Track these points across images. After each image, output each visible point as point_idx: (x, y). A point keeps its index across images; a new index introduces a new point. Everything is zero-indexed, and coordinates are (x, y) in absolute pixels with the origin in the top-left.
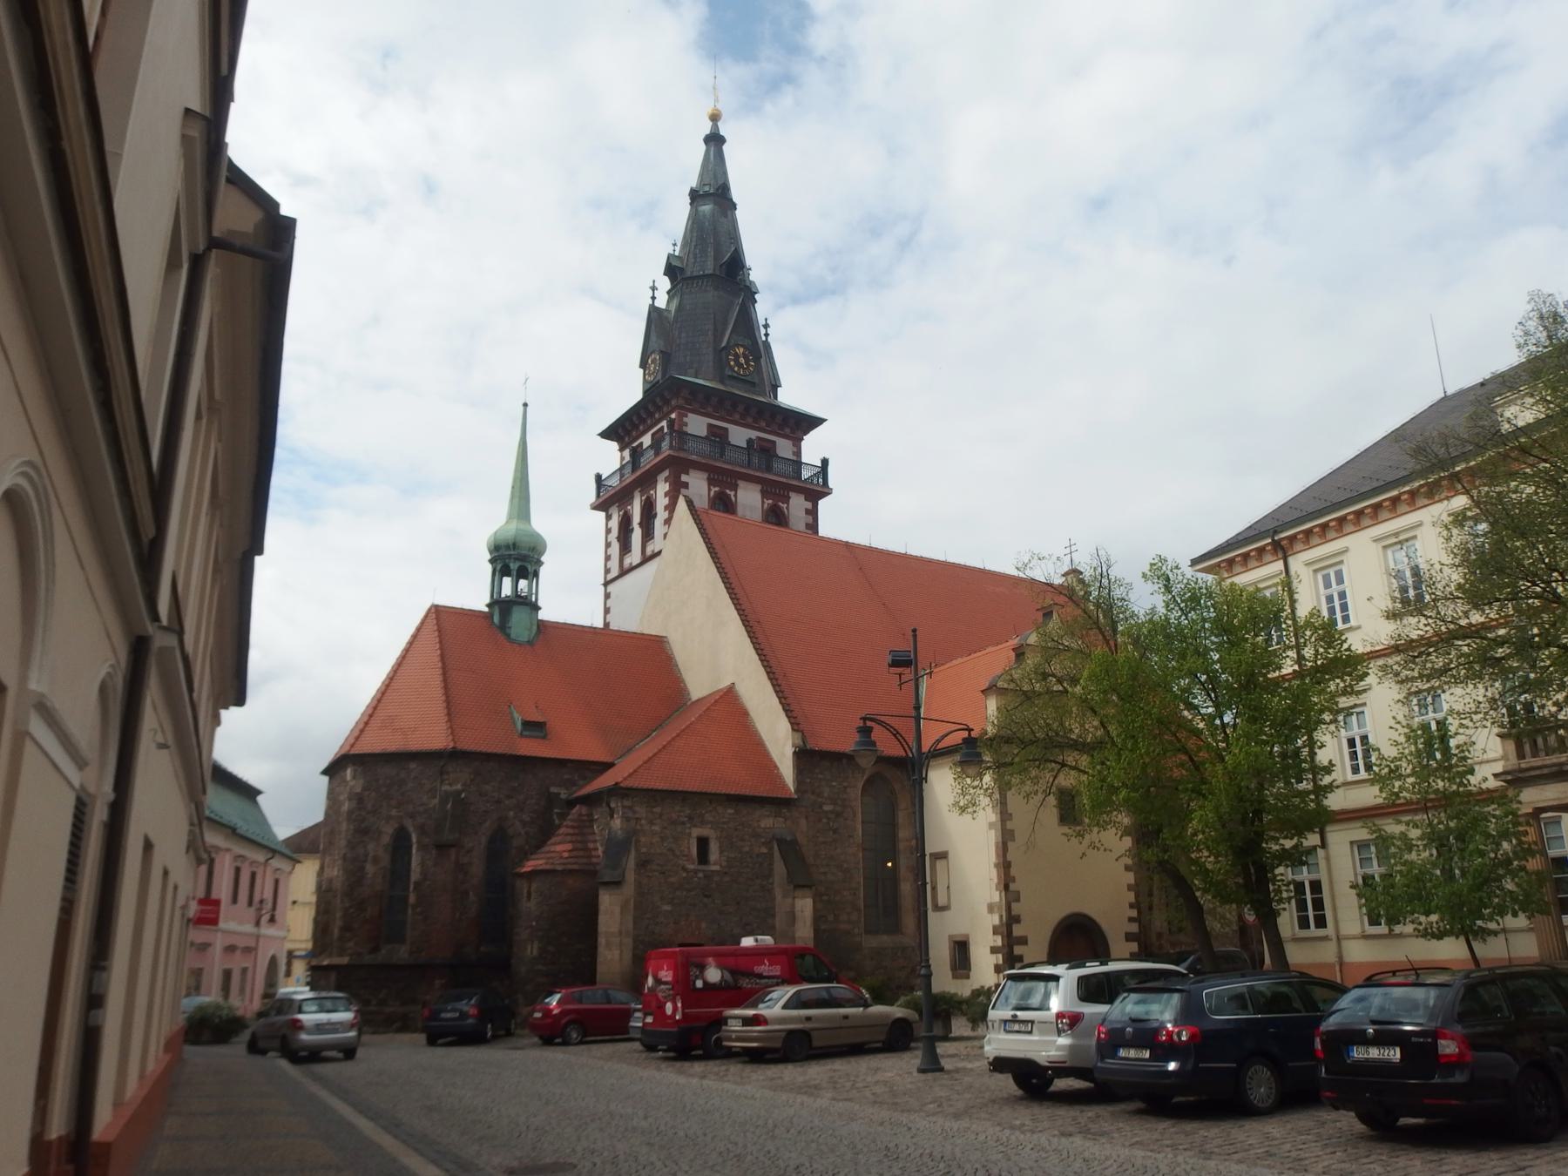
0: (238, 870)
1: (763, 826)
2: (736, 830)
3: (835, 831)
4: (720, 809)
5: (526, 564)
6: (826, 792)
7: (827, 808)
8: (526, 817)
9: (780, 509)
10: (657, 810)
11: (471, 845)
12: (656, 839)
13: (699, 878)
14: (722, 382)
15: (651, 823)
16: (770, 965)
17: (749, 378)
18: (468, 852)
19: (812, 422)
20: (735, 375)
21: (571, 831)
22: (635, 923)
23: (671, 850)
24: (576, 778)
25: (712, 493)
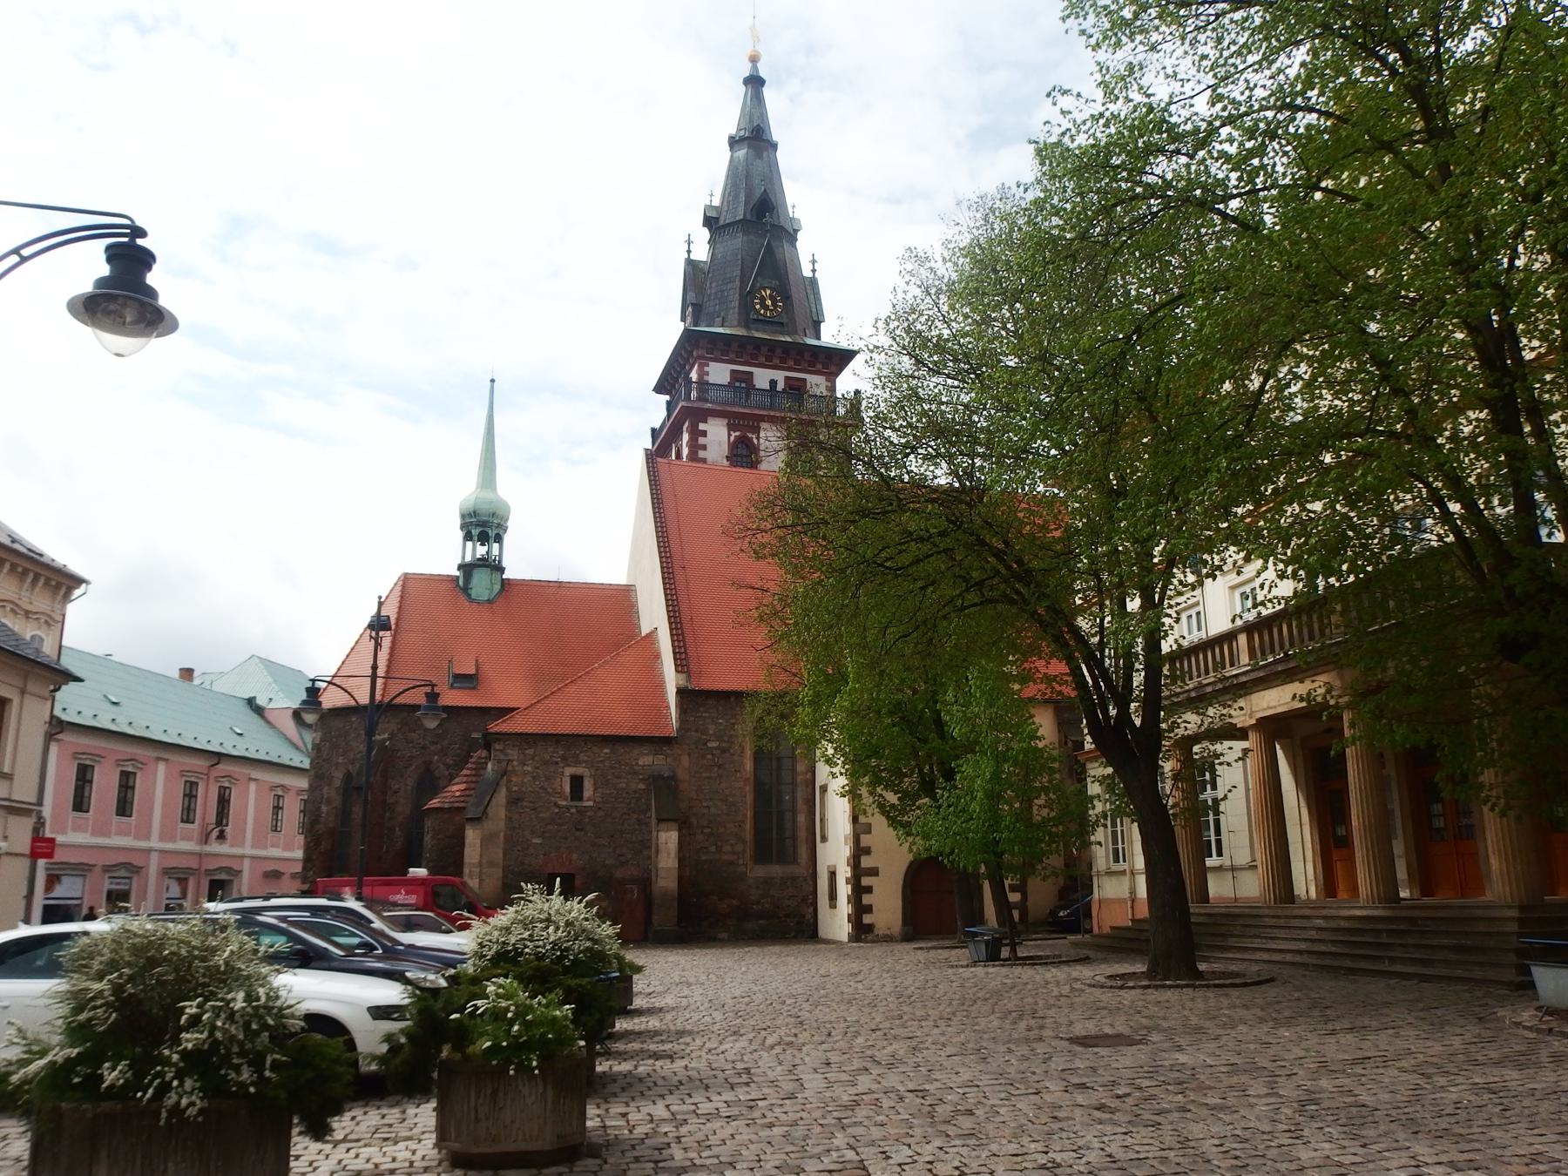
1: (641, 763)
3: (720, 766)
4: (596, 749)
6: (712, 729)
7: (711, 745)
8: (449, 761)
10: (530, 751)
12: (528, 779)
14: (747, 327)
16: (407, 894)
17: (776, 320)
22: (505, 854)
25: (732, 438)
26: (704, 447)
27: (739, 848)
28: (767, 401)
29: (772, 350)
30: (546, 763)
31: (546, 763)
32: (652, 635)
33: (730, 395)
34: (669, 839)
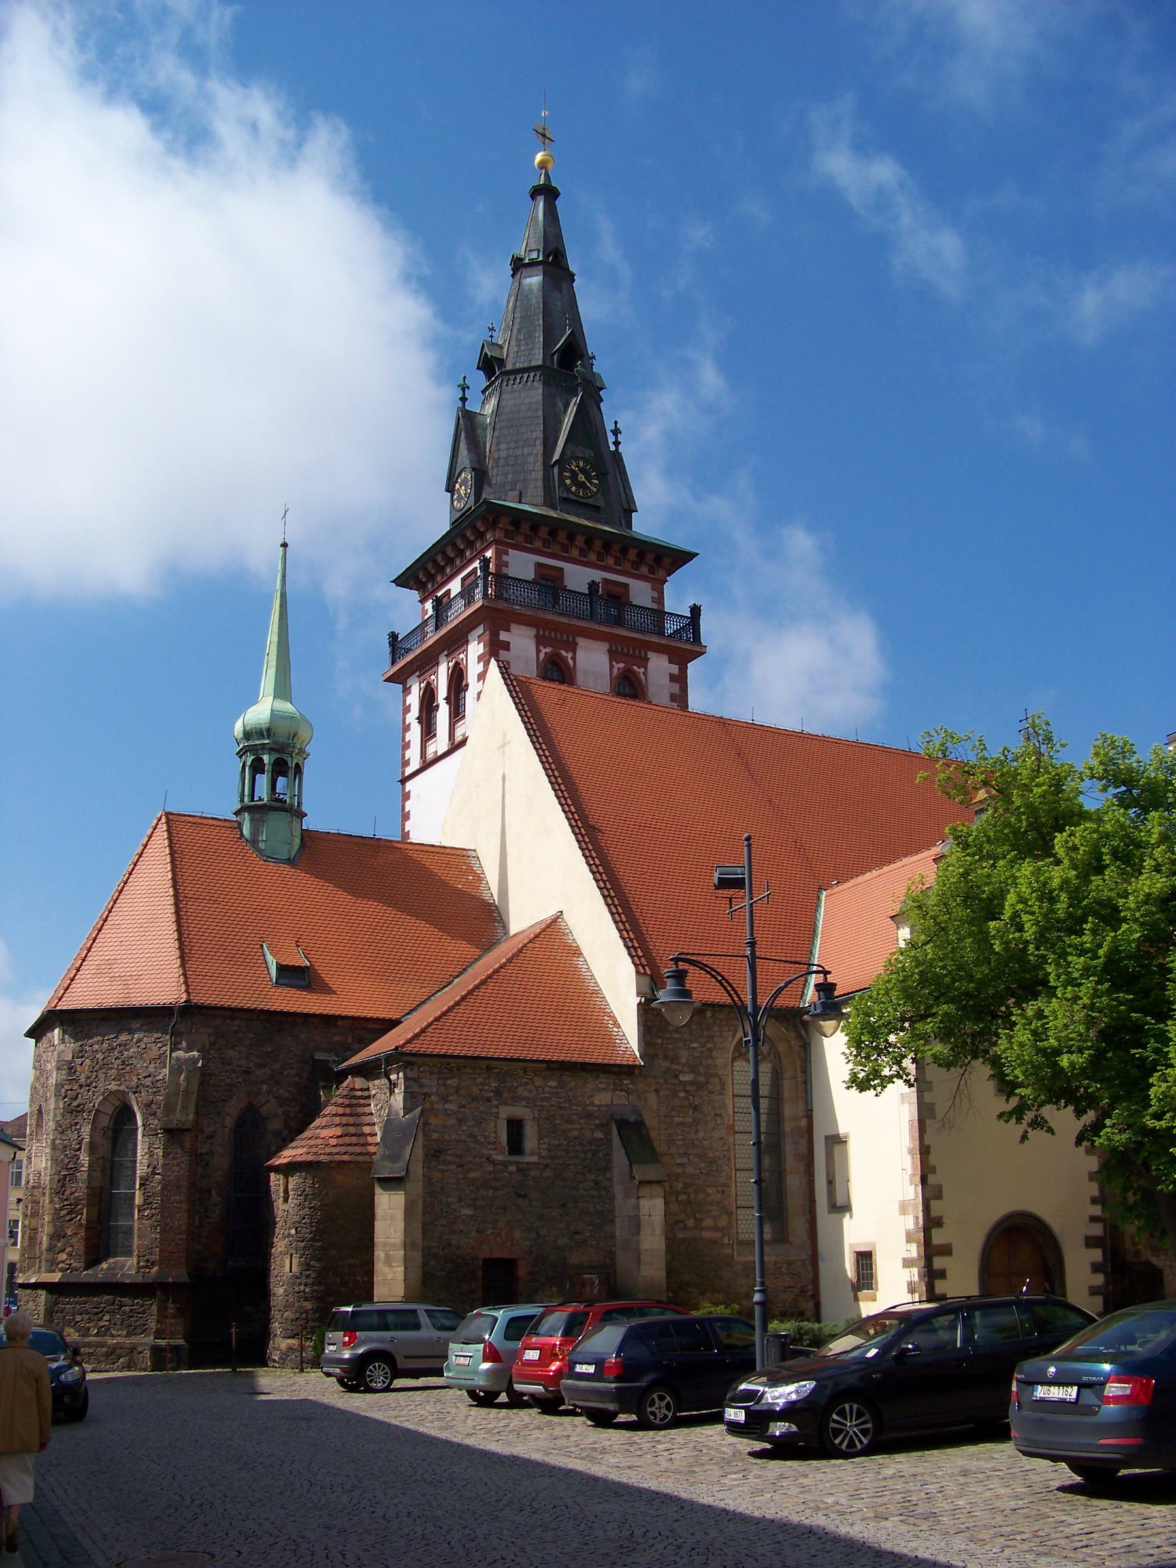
4: (539, 1081)
5: (285, 757)
6: (684, 1055)
11: (212, 1128)
12: (452, 1121)
13: (511, 1173)
17: (590, 501)
20: (572, 496)
21: (341, 1110)
24: (350, 1040)
25: (542, 656)
28: (586, 607)
30: (475, 1099)
31: (475, 1099)
33: (534, 595)
34: (653, 1208)
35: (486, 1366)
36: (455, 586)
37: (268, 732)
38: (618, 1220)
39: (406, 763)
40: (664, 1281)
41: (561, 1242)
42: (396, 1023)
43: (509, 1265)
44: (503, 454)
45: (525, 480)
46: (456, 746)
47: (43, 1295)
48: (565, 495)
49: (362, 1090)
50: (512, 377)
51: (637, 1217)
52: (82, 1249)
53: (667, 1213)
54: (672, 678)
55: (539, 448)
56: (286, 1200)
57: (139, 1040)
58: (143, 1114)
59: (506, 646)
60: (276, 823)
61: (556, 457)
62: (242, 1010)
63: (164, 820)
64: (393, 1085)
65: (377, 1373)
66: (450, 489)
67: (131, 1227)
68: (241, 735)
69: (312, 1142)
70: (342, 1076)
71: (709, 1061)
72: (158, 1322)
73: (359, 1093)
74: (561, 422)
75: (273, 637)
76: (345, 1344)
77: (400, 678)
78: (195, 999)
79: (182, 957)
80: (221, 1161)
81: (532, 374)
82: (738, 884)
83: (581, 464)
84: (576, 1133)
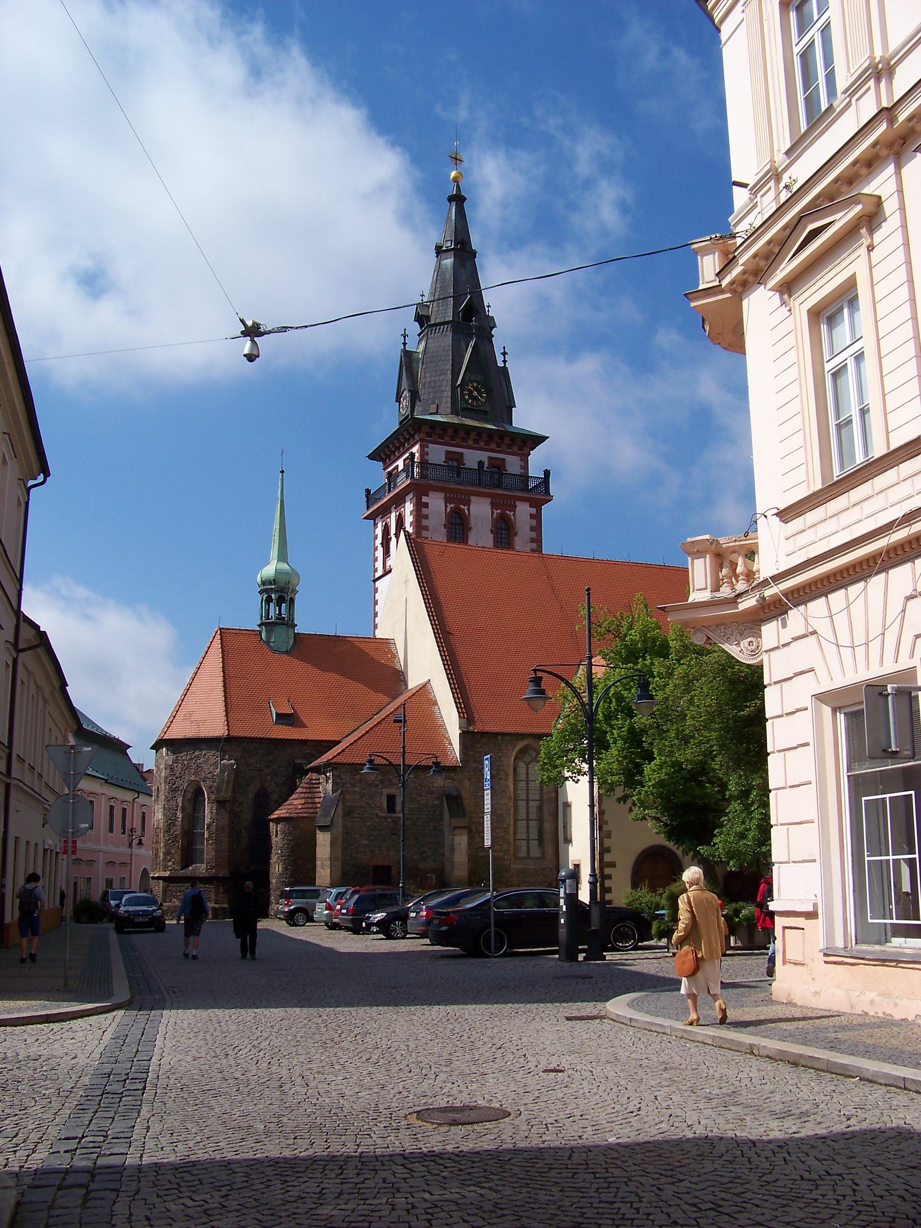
0: (112, 807)
2: (416, 789)
5: (283, 594)
9: (508, 516)
11: (242, 799)
13: (389, 823)
15: (354, 786)
17: (481, 408)
18: (241, 804)
19: (538, 440)
20: (469, 406)
21: (304, 790)
23: (367, 803)
24: (314, 752)
25: (448, 510)
26: (426, 517)
27: (505, 847)
29: (479, 435)
32: (424, 688)
35: (326, 912)
36: (400, 463)
37: (273, 581)
38: (446, 847)
39: (376, 570)
40: (467, 876)
41: (414, 857)
42: (339, 742)
43: (388, 868)
44: (428, 380)
45: (441, 397)
46: (387, 572)
47: (161, 882)
48: (465, 406)
49: (316, 780)
50: (434, 328)
51: (453, 845)
52: (179, 861)
53: (469, 844)
54: (532, 516)
55: (449, 377)
56: (276, 836)
57: (205, 755)
58: (207, 793)
59: (426, 505)
60: (280, 631)
61: (459, 383)
62: (256, 738)
63: (219, 633)
64: (328, 779)
65: (300, 917)
66: (398, 400)
67: (204, 849)
68: (260, 583)
69: (290, 807)
70: (307, 772)
71: (499, 763)
72: (215, 896)
73: (314, 782)
74: (464, 358)
75: (277, 526)
76: (286, 904)
77: (372, 517)
78: (232, 734)
79: (226, 711)
80: (247, 816)
81: (446, 326)
82: (400, 721)
83: (475, 385)
84: (424, 802)
